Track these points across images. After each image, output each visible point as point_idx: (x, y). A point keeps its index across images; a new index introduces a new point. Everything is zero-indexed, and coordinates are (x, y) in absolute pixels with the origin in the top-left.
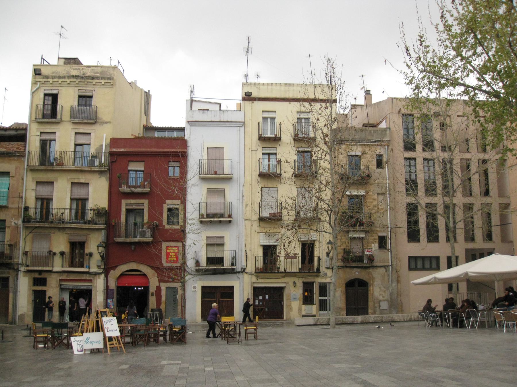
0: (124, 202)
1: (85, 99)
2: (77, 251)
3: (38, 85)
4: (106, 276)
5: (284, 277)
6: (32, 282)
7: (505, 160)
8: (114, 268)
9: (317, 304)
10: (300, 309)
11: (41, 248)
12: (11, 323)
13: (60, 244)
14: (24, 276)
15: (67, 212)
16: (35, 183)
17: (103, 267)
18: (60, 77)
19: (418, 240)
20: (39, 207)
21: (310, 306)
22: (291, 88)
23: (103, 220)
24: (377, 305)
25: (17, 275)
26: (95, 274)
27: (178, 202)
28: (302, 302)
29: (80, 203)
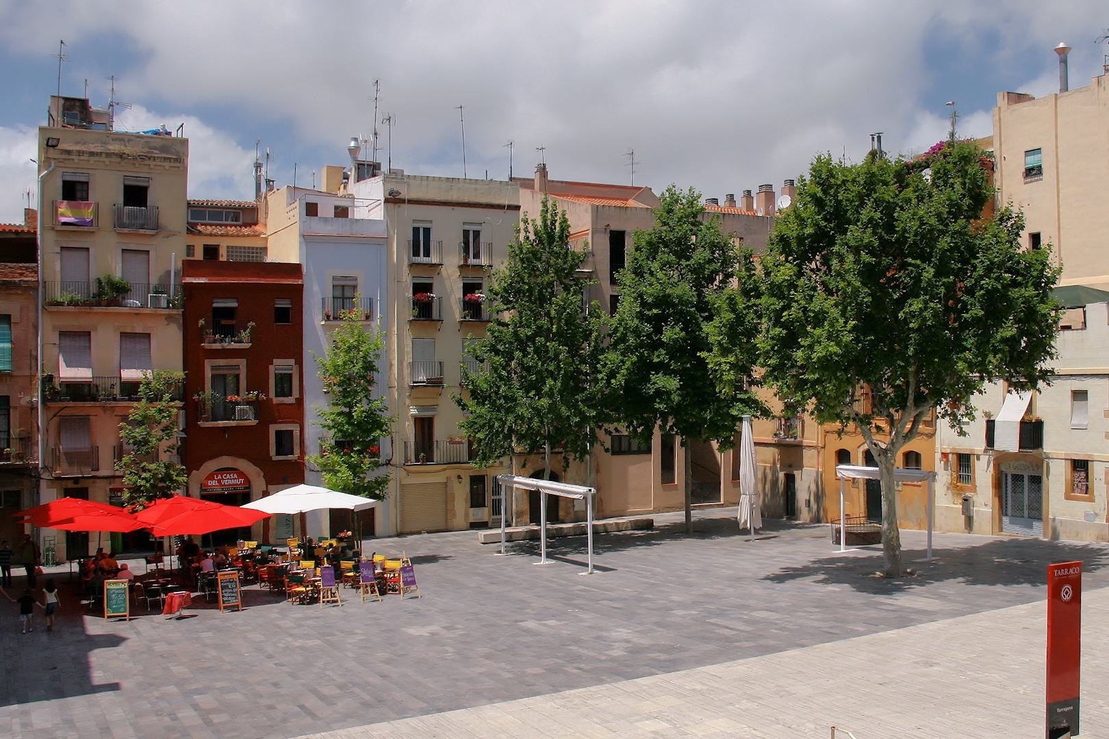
0: (208, 365)
7: (703, 419)
10: (467, 515)
19: (431, 285)
25: (38, 486)
27: (292, 362)
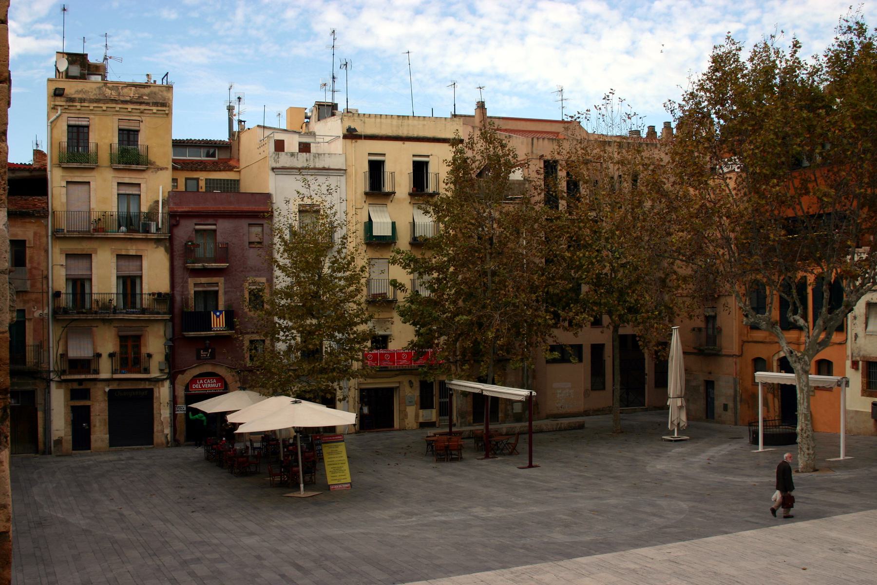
1: (128, 136)
2: (130, 354)
3: (59, 112)
4: (173, 383)
5: (397, 375)
6: (69, 396)
8: (183, 372)
9: (438, 408)
10: (417, 416)
11: (79, 350)
12: (44, 453)
13: (107, 343)
14: (57, 388)
15: (114, 297)
16: (64, 256)
17: (167, 371)
18: (92, 101)
20: (70, 291)
21: (428, 411)
22: (406, 122)
23: (164, 308)
24: (509, 407)
25: (49, 387)
26: (157, 381)
28: (419, 407)
29: (129, 284)
